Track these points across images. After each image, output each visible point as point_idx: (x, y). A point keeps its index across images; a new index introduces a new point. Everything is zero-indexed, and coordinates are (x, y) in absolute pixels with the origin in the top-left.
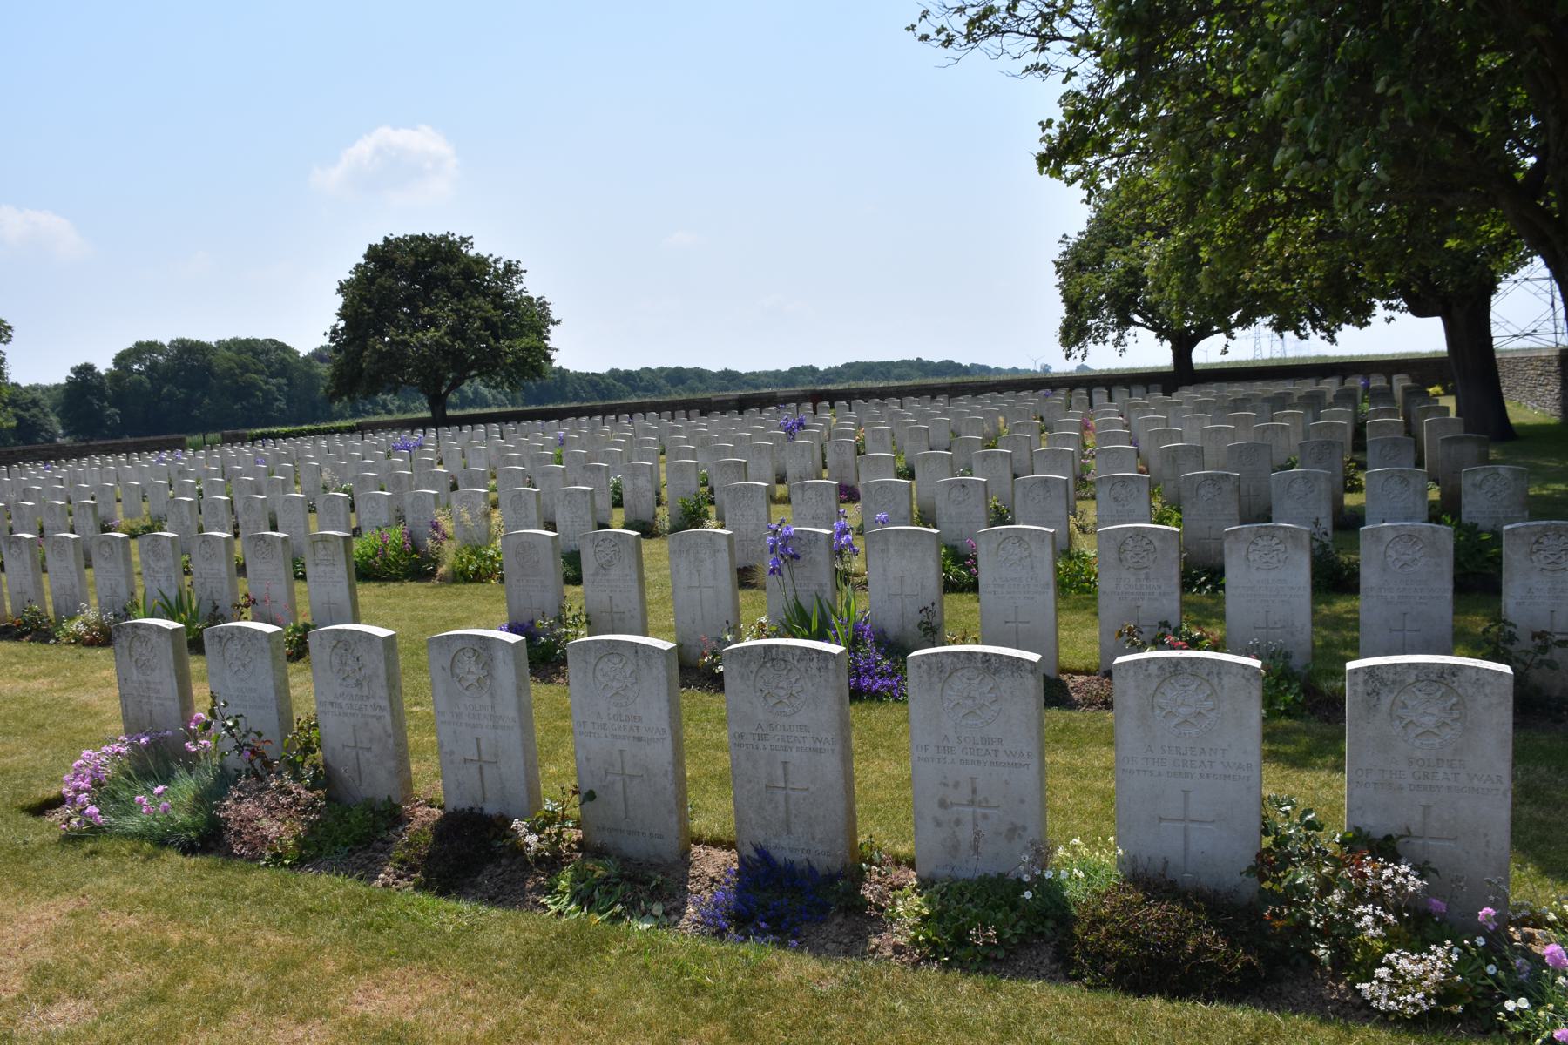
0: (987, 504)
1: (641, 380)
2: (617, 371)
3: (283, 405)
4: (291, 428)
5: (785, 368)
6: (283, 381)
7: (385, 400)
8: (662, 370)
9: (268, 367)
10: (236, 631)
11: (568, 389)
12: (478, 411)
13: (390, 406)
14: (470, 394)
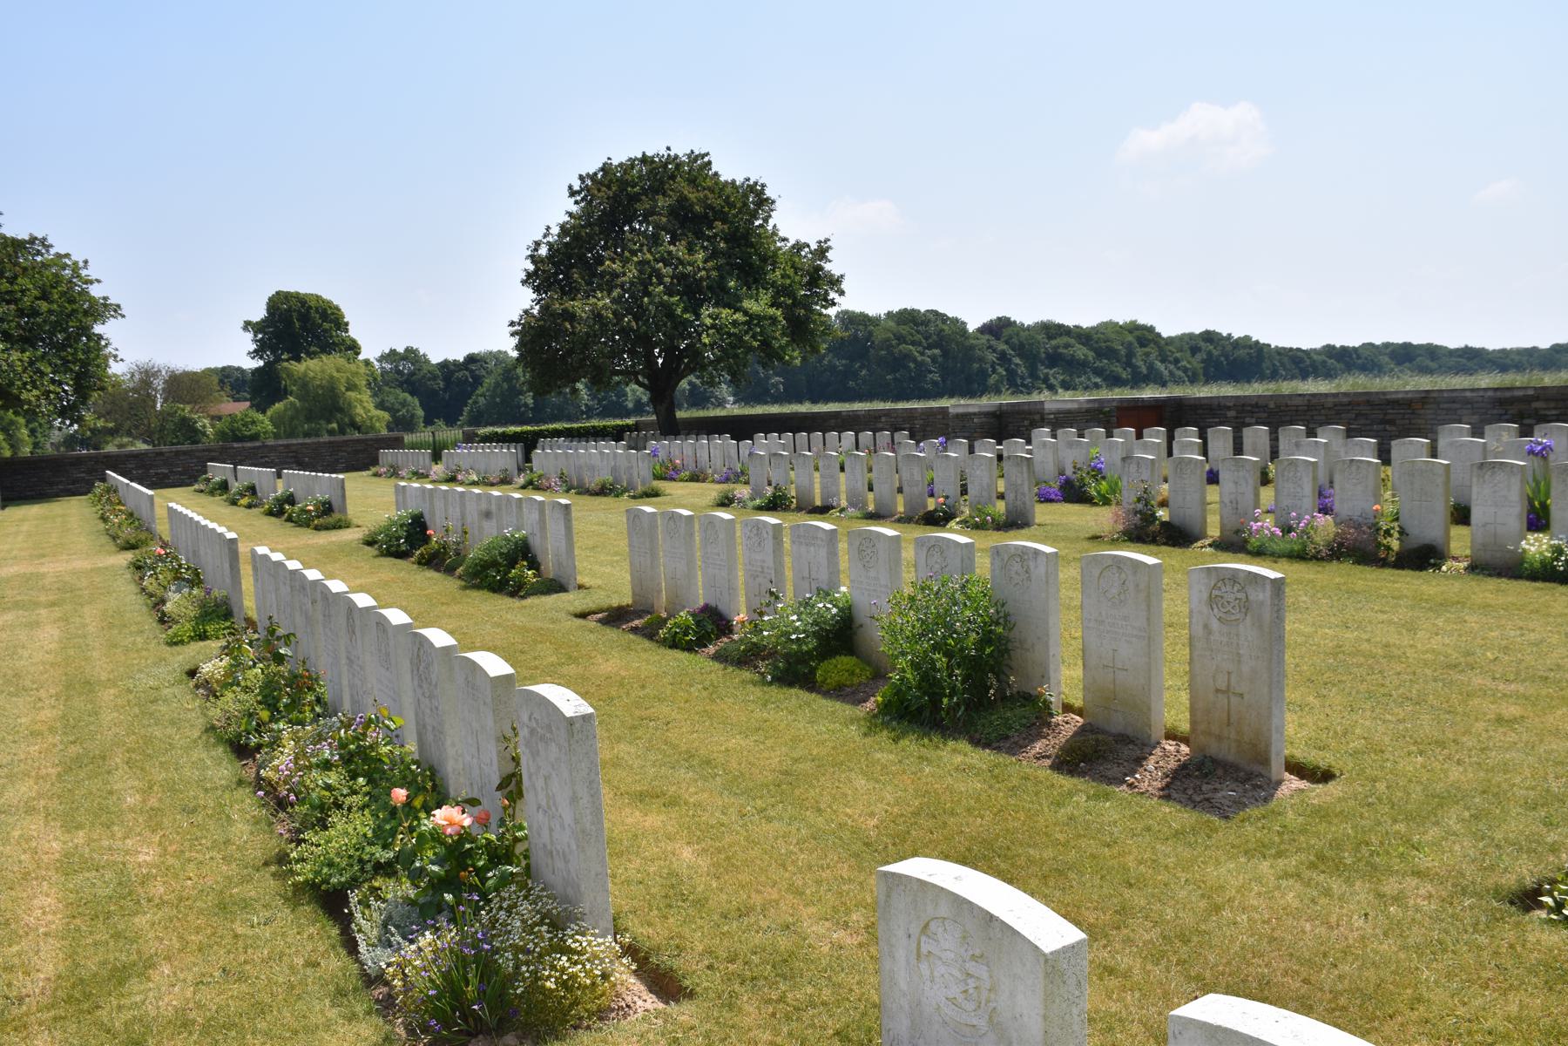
0: (1277, 491)
1: (1359, 357)
2: (1334, 347)
3: (936, 377)
4: (529, 428)
5: (1544, 344)
6: (937, 351)
7: (1047, 374)
8: (1387, 345)
9: (926, 339)
10: (1242, 575)
11: (1264, 365)
12: (775, 409)
13: (1052, 380)
14: (1144, 370)
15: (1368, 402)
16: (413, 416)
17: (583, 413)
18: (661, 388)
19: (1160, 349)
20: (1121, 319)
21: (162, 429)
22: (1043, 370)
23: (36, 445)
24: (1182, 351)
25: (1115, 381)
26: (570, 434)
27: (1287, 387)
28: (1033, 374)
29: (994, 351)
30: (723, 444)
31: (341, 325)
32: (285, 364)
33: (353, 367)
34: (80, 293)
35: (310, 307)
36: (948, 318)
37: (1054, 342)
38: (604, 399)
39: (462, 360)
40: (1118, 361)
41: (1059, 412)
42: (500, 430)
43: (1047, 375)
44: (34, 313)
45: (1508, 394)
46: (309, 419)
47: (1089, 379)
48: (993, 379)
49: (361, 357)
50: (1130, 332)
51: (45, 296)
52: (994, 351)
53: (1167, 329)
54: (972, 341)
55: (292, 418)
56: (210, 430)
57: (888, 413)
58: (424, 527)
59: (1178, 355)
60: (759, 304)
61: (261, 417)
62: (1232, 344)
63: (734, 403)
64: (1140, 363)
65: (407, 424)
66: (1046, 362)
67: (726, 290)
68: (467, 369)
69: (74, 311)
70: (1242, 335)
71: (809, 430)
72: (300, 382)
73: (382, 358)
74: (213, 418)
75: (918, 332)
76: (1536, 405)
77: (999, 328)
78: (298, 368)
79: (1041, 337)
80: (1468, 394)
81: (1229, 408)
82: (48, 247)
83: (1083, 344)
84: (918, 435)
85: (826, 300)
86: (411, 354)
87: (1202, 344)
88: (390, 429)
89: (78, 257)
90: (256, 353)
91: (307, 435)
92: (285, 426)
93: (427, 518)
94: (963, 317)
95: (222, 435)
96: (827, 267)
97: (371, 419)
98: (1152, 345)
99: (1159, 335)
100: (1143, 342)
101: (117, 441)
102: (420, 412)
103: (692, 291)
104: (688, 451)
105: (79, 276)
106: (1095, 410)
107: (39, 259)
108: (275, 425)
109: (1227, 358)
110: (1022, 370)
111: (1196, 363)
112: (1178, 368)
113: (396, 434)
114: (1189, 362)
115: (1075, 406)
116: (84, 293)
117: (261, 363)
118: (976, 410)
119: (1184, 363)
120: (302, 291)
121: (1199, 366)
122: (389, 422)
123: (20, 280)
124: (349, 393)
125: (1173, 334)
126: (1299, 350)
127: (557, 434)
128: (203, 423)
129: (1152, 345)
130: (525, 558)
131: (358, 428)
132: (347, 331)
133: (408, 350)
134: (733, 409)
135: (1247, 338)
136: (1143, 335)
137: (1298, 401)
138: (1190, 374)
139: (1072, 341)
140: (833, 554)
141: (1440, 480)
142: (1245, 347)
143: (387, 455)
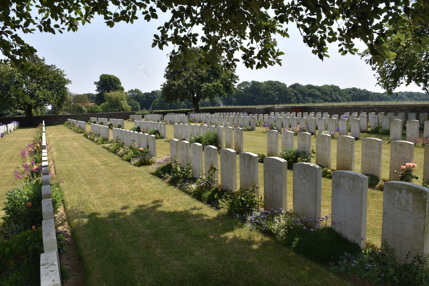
3: (277, 99)
6: (278, 92)
8: (405, 92)
11: (369, 97)
14: (335, 98)
15: (343, 108)
16: (137, 107)
17: (182, 107)
18: (196, 101)
19: (340, 93)
20: (329, 84)
21: (74, 110)
22: (307, 98)
23: (42, 113)
24: (346, 93)
25: (326, 101)
26: (175, 112)
27: (377, 103)
28: (304, 99)
29: (293, 92)
30: (209, 115)
31: (119, 83)
32: (105, 93)
33: (122, 94)
34: (62, 78)
35: (111, 78)
36: (281, 83)
37: (310, 90)
38: (188, 103)
39: (150, 92)
40: (328, 96)
41: (278, 109)
42: (158, 111)
43: (308, 99)
44: (53, 82)
45: (369, 106)
46: (111, 108)
47: (320, 101)
48: (292, 100)
49: (124, 92)
50: (332, 88)
51: (55, 79)
52: (293, 92)
53: (342, 87)
54: (287, 90)
55: (107, 107)
56: (86, 110)
57: (246, 108)
58: (140, 129)
59: (345, 94)
60: (218, 83)
61: (99, 107)
62: (360, 91)
63: (223, 105)
64: (334, 96)
65: (136, 109)
66: (308, 95)
67: (210, 79)
68: (152, 95)
69: (61, 82)
70: (364, 89)
71: (226, 112)
72: (109, 98)
73: (129, 92)
74: (86, 107)
75: (273, 87)
76: (375, 109)
77: (295, 86)
78: (109, 94)
79: (307, 89)
80: (362, 106)
81: (316, 109)
82: (55, 67)
83: (318, 91)
84: (249, 113)
85: (235, 81)
86: (137, 91)
87: (352, 91)
88: (131, 111)
89: (62, 69)
90: (98, 90)
91: (110, 111)
92: (105, 109)
93: (140, 127)
94: (285, 83)
95: (89, 111)
96: (235, 74)
97: (127, 108)
98: (338, 91)
99: (340, 89)
100: (335, 90)
101: (63, 112)
102: (139, 106)
103: (203, 80)
104: (198, 116)
105: (62, 74)
106: (285, 108)
107: (53, 70)
108: (102, 109)
109: (359, 95)
110: (301, 98)
111: (350, 96)
112: (345, 98)
113: (133, 112)
114: (348, 96)
115: (281, 108)
116: (63, 77)
117: (98, 93)
118: (261, 108)
119: (346, 96)
120: (110, 74)
121: (351, 98)
122: (131, 109)
123: (49, 75)
124: (121, 101)
125: (344, 88)
126: (379, 93)
127: (172, 112)
128: (84, 108)
129: (338, 91)
130: (157, 133)
131: (123, 110)
132: (121, 85)
133: (135, 89)
134: (222, 107)
135: (365, 90)
136: (335, 89)
137: (330, 107)
138: (348, 99)
139: (315, 90)
140: (200, 129)
141: (314, 121)
142: (364, 92)
143: (131, 116)
